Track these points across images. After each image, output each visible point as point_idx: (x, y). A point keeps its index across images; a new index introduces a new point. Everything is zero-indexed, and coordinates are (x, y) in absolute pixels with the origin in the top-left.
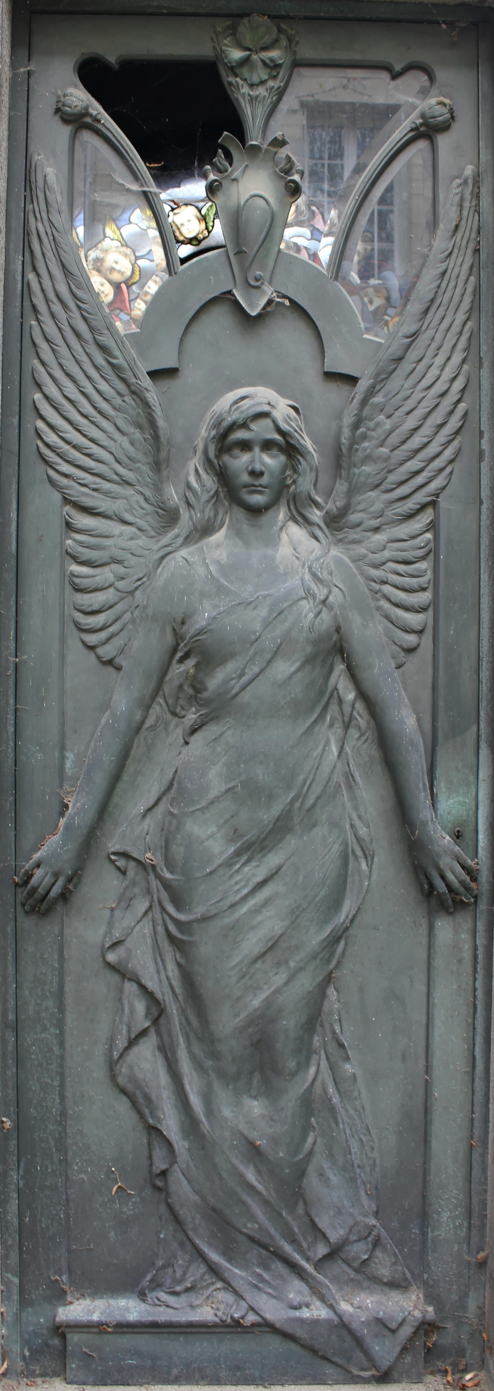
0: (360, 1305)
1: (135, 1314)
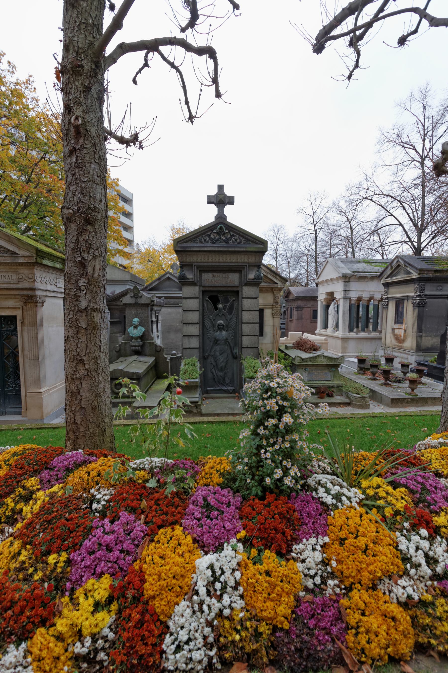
0: (229, 388)
1: (102, 592)
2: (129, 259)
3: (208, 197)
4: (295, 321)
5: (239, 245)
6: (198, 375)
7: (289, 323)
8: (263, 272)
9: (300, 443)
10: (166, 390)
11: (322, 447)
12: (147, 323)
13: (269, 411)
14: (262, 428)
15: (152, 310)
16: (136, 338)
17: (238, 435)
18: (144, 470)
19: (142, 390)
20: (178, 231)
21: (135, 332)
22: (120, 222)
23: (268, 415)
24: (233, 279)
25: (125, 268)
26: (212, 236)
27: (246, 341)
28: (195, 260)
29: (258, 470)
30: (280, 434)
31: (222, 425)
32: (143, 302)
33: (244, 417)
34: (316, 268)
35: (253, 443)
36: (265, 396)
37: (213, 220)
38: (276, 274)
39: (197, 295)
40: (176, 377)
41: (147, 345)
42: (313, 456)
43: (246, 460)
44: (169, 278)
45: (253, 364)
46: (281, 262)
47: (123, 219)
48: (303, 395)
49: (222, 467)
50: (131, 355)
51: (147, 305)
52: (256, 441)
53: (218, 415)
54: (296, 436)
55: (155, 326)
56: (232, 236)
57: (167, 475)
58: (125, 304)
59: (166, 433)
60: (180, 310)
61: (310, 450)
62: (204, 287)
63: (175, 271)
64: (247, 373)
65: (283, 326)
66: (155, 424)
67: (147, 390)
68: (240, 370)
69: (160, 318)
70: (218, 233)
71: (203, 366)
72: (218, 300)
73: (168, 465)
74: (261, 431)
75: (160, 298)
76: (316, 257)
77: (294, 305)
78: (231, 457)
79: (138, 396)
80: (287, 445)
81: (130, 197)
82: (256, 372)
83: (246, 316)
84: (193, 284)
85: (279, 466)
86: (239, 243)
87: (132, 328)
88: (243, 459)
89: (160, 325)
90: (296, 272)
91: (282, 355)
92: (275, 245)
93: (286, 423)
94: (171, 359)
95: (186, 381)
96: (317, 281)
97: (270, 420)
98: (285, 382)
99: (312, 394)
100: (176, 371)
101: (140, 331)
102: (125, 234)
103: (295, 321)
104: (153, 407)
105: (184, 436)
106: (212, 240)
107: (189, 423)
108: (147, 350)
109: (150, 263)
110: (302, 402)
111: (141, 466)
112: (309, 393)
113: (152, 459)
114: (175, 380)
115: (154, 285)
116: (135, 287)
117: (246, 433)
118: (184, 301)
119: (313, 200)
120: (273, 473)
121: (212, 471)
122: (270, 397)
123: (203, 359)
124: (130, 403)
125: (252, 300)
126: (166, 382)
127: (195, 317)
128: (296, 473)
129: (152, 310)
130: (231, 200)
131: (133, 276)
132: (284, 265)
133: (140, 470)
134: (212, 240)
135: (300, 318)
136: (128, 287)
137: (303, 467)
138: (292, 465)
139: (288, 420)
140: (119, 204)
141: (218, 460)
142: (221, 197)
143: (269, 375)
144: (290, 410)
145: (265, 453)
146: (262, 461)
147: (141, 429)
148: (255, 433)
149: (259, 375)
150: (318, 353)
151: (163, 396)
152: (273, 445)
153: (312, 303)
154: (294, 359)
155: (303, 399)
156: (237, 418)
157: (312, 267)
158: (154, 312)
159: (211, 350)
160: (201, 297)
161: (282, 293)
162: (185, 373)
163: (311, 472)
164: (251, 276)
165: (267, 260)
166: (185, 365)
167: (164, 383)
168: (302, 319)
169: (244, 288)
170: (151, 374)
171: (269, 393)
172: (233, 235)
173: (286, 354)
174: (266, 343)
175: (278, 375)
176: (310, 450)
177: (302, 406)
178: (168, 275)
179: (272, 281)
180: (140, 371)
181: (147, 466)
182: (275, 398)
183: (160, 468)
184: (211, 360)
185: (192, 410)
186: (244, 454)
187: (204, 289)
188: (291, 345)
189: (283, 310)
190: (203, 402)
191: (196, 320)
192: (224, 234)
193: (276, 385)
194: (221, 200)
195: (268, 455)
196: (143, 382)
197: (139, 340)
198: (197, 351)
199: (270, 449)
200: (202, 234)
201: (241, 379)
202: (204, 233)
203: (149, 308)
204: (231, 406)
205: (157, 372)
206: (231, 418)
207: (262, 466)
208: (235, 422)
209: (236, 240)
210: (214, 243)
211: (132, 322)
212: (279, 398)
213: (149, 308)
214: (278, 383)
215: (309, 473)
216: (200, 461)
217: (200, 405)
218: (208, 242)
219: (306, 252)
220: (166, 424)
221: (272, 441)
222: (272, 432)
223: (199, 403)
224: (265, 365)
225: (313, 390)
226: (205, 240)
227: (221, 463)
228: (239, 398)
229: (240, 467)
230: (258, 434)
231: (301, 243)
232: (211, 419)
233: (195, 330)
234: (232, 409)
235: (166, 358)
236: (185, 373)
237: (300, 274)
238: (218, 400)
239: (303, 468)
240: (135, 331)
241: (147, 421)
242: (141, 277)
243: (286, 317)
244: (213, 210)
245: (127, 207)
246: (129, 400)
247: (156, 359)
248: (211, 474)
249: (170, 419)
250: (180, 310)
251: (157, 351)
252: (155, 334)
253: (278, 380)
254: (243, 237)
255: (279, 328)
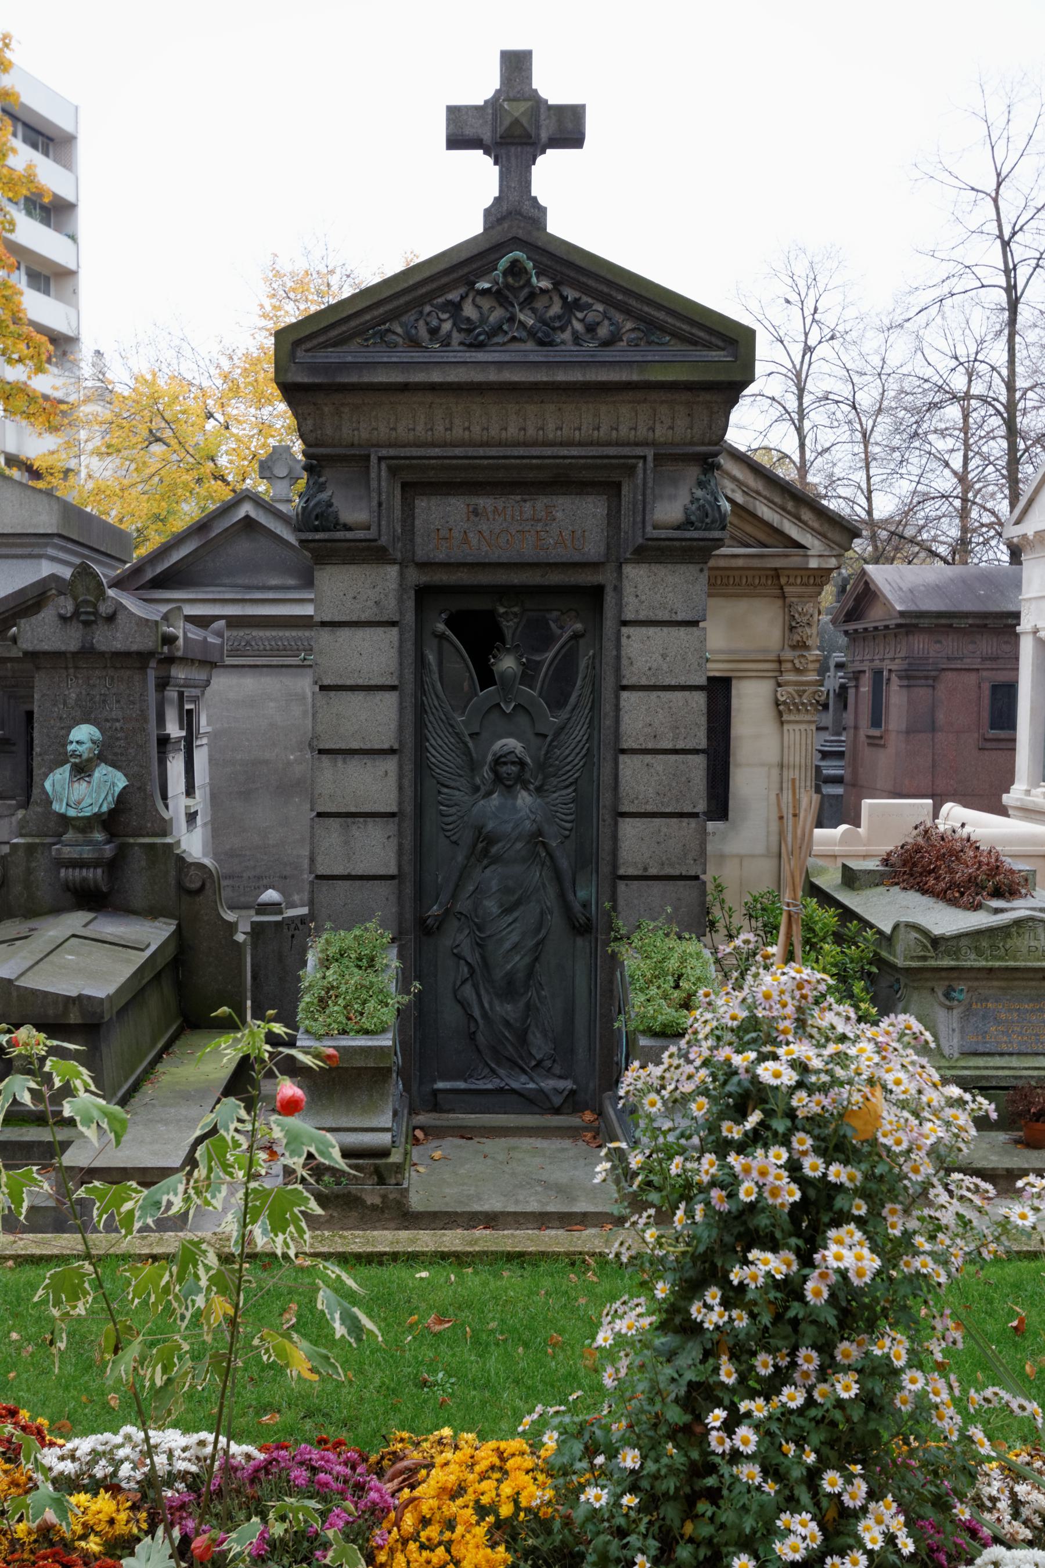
0: (549, 1084)
2: (53, 429)
3: (454, 113)
4: (895, 742)
5: (607, 355)
6: (388, 1015)
7: (867, 752)
8: (728, 487)
9: (913, 1382)
10: (227, 1092)
11: (1033, 1407)
12: (140, 752)
13: (751, 1207)
14: (713, 1295)
15: (163, 684)
16: (85, 825)
17: (594, 1327)
18: (114, 1488)
19: (103, 1086)
20: (301, 286)
21: (79, 794)
22: (16, 249)
23: (745, 1229)
24: (575, 525)
25: (35, 474)
26: (469, 311)
27: (637, 844)
28: (383, 432)
29: (690, 1513)
30: (810, 1330)
31: (509, 1275)
32: (118, 646)
33: (622, 1234)
34: (1013, 461)
35: (669, 1371)
36: (733, 1131)
37: (475, 227)
38: (799, 499)
39: (390, 612)
40: (278, 1028)
41: (138, 861)
42: (985, 1449)
43: (630, 1459)
44: (248, 523)
45: (673, 964)
46: (826, 437)
47: (31, 233)
48: (933, 1131)
49: (507, 1489)
50: (57, 910)
51: (140, 659)
52: (683, 1361)
53: (491, 1220)
54: (893, 1346)
55: (176, 767)
56: (571, 307)
57: (228, 1522)
58: (33, 656)
59: (221, 1307)
60: (304, 684)
61: (969, 1419)
62: (423, 566)
63: (281, 489)
64: (644, 1005)
65: (831, 768)
66: (168, 1258)
67: (135, 1088)
68: (608, 992)
69: (204, 723)
70: (498, 295)
71: (416, 968)
72: (503, 640)
73: (230, 1468)
74: (710, 1312)
75: (202, 622)
76: (1011, 406)
77: (891, 658)
78: (550, 1440)
79: (88, 1121)
80: (846, 1387)
81: (67, 126)
82: (687, 1005)
83: (639, 717)
84: (369, 553)
85: (804, 1496)
86: (606, 343)
87: (62, 774)
88: (612, 1454)
89: (201, 758)
90: (904, 487)
91: (827, 918)
92: (796, 350)
93: (843, 1274)
94: (258, 931)
95: (327, 1047)
96: (1013, 532)
97: (754, 1254)
98: (840, 1058)
99: (982, 1123)
100: (278, 996)
101: (107, 784)
102: (39, 307)
103: (895, 742)
104: (165, 1172)
105: (312, 1326)
106: (467, 327)
107: (343, 1259)
108: (138, 883)
109: (157, 448)
110: (927, 1169)
111: (100, 1470)
112: (963, 1119)
113: (155, 1436)
114: (272, 1039)
115: (176, 556)
116: (83, 572)
117: (630, 1319)
118: (325, 637)
119: (997, 114)
120: (771, 1532)
121: (452, 1508)
122: (757, 1138)
123: (419, 937)
124: (46, 1154)
125: (678, 635)
126: (223, 1053)
127: (377, 719)
128: (890, 1539)
129: (163, 684)
130: (567, 128)
131: (71, 512)
132: (837, 453)
133: (95, 1487)
134: (467, 327)
135: (923, 725)
136: (46, 569)
137: (927, 1509)
138: (873, 1495)
139: (849, 1260)
140: (12, 161)
141: (486, 1456)
142: (518, 110)
143: (752, 1023)
144: (861, 1209)
145: (729, 1428)
146: (712, 1469)
147: (99, 1284)
148: (675, 1321)
149: (701, 1021)
150: (1019, 909)
151: (209, 1119)
152: (770, 1388)
153: (986, 645)
154: (887, 940)
155: (934, 1152)
156: (587, 1239)
157: (987, 461)
158: (172, 694)
159: (458, 887)
160: (410, 617)
161: (828, 596)
162: (323, 1003)
163: (973, 1532)
164: (670, 509)
165: (752, 426)
166: (325, 963)
167: (217, 1052)
168: (933, 728)
169: (630, 571)
170: (153, 1002)
171: (754, 1119)
172: (577, 305)
173: (847, 914)
174: (743, 852)
175: (801, 1023)
176: (969, 1419)
177: (927, 1185)
178: (246, 509)
179: (777, 538)
180: (101, 989)
181: (125, 1470)
182: (786, 1142)
183: (193, 1482)
184: (457, 937)
185: (357, 1192)
186: (619, 1428)
187: (424, 579)
188: (873, 865)
189: (833, 681)
190: (416, 1153)
191: (386, 738)
192: (532, 296)
193: (789, 1077)
194: (517, 126)
195: (746, 1438)
196: (116, 1044)
197: (99, 836)
198: (384, 890)
199: (757, 1408)
200: (419, 302)
201: (610, 1037)
202: (429, 298)
203: (151, 675)
204: (559, 1174)
205: (185, 995)
206: (555, 1240)
207: (714, 1496)
208: (575, 1261)
209: (591, 329)
210: (479, 346)
211: (64, 742)
212: (802, 1141)
213: (151, 675)
214: (800, 1066)
215: (964, 1538)
216: (396, 1457)
217: (399, 1168)
218: (446, 343)
219: (959, 382)
220: (226, 1259)
221: (764, 1365)
222: (766, 1319)
223: (395, 1158)
224: (738, 969)
225: (988, 1107)
226: (434, 332)
227: (500, 1469)
228: (601, 1134)
229: (596, 1496)
230: (695, 1329)
231: (932, 337)
232: (453, 1240)
233: (376, 785)
234: (563, 1191)
235: (232, 927)
236: (323, 1003)
237: (926, 498)
238: (491, 1145)
239: (929, 1511)
240: (81, 788)
241: (129, 1243)
242: (112, 518)
243: (848, 718)
244: (479, 177)
245: (50, 176)
246: (43, 1134)
247: (179, 931)
248: (450, 1525)
249: (245, 1239)
250: (304, 684)
251: (182, 889)
252: (178, 803)
253: (802, 1050)
254: (627, 311)
255: (808, 780)
